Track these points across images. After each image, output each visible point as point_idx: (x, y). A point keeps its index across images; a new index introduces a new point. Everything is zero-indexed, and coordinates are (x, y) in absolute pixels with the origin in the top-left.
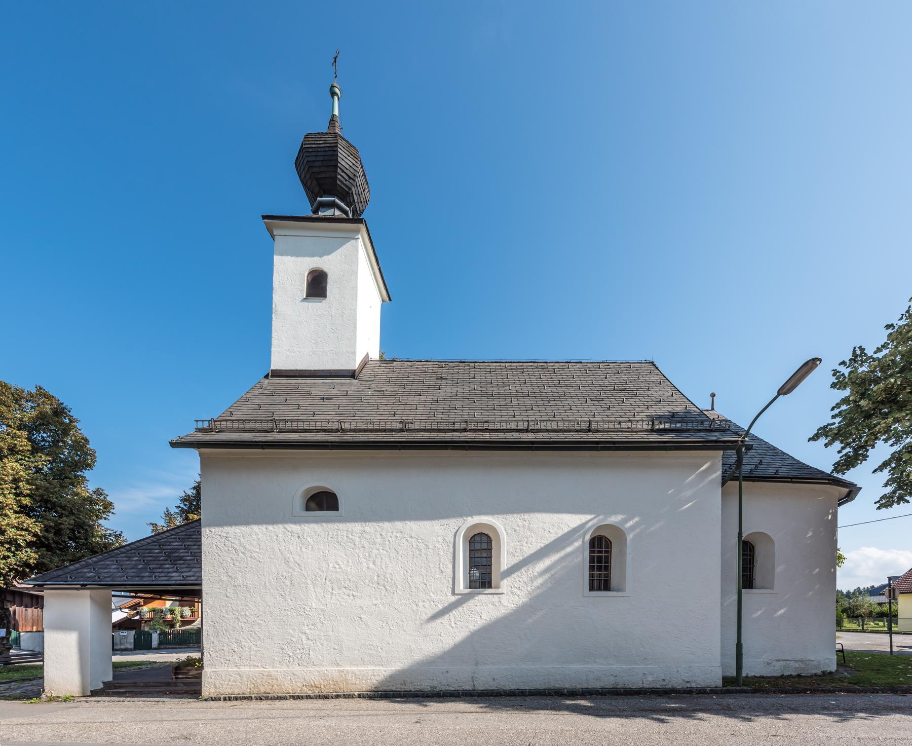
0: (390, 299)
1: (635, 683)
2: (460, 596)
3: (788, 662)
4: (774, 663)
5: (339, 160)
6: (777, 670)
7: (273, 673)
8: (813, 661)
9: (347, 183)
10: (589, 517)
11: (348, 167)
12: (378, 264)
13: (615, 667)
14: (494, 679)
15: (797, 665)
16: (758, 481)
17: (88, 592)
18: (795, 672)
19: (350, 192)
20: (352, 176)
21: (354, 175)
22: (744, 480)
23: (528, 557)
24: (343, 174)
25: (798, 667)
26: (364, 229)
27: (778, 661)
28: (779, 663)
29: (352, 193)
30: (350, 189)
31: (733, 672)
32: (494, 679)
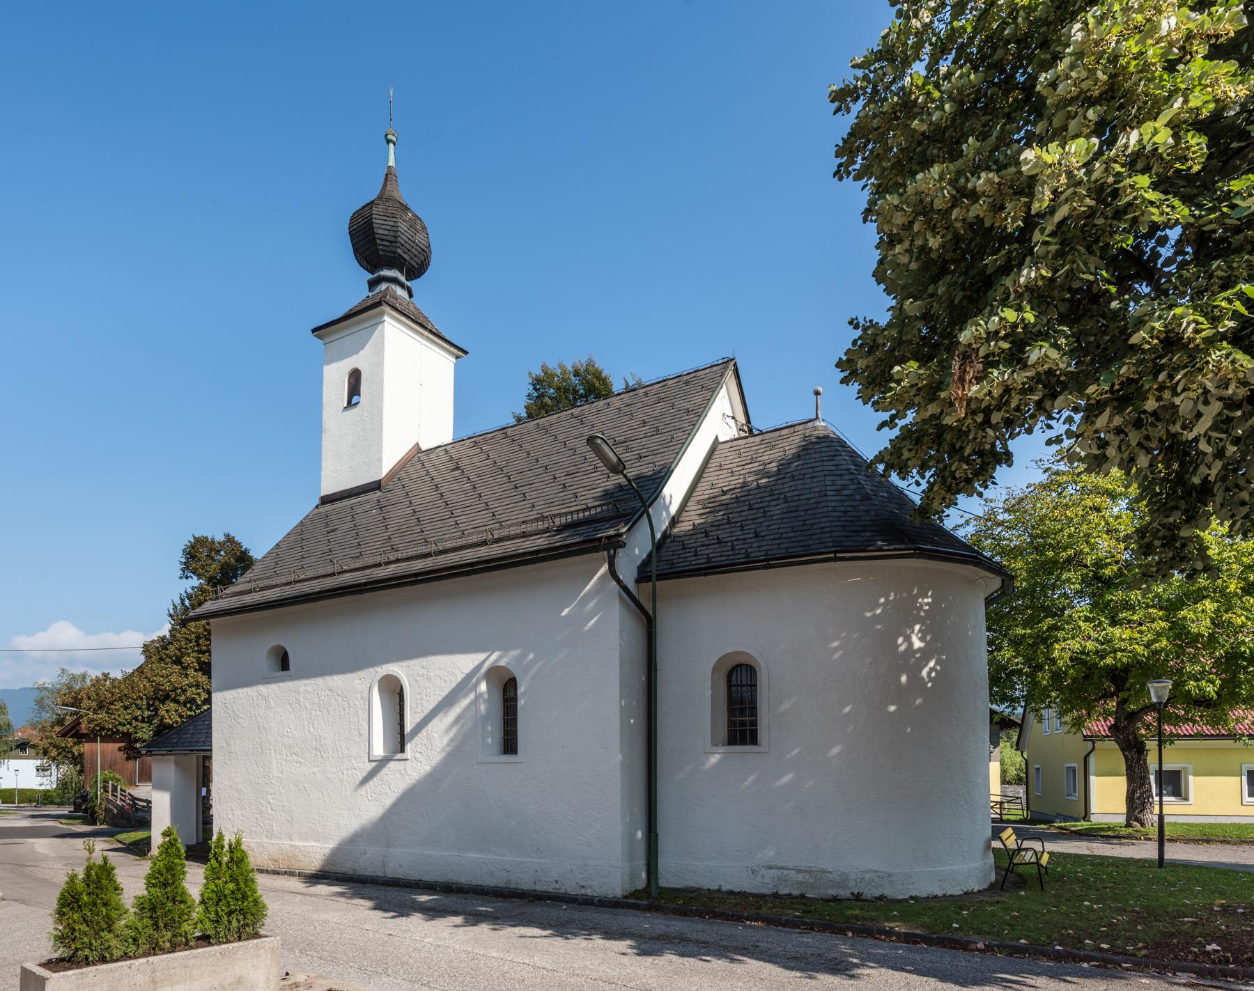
1: (526, 883)
2: (377, 763)
3: (785, 872)
4: (763, 871)
5: (376, 231)
7: (251, 844)
8: (830, 872)
9: (391, 249)
10: (481, 657)
11: (386, 233)
14: (400, 866)
15: (800, 877)
16: (690, 576)
17: (173, 758)
18: (796, 889)
20: (393, 239)
21: (395, 237)
22: (658, 580)
23: (429, 714)
25: (802, 882)
26: (387, 309)
27: (770, 868)
28: (770, 871)
29: (399, 255)
31: (641, 882)
32: (400, 866)
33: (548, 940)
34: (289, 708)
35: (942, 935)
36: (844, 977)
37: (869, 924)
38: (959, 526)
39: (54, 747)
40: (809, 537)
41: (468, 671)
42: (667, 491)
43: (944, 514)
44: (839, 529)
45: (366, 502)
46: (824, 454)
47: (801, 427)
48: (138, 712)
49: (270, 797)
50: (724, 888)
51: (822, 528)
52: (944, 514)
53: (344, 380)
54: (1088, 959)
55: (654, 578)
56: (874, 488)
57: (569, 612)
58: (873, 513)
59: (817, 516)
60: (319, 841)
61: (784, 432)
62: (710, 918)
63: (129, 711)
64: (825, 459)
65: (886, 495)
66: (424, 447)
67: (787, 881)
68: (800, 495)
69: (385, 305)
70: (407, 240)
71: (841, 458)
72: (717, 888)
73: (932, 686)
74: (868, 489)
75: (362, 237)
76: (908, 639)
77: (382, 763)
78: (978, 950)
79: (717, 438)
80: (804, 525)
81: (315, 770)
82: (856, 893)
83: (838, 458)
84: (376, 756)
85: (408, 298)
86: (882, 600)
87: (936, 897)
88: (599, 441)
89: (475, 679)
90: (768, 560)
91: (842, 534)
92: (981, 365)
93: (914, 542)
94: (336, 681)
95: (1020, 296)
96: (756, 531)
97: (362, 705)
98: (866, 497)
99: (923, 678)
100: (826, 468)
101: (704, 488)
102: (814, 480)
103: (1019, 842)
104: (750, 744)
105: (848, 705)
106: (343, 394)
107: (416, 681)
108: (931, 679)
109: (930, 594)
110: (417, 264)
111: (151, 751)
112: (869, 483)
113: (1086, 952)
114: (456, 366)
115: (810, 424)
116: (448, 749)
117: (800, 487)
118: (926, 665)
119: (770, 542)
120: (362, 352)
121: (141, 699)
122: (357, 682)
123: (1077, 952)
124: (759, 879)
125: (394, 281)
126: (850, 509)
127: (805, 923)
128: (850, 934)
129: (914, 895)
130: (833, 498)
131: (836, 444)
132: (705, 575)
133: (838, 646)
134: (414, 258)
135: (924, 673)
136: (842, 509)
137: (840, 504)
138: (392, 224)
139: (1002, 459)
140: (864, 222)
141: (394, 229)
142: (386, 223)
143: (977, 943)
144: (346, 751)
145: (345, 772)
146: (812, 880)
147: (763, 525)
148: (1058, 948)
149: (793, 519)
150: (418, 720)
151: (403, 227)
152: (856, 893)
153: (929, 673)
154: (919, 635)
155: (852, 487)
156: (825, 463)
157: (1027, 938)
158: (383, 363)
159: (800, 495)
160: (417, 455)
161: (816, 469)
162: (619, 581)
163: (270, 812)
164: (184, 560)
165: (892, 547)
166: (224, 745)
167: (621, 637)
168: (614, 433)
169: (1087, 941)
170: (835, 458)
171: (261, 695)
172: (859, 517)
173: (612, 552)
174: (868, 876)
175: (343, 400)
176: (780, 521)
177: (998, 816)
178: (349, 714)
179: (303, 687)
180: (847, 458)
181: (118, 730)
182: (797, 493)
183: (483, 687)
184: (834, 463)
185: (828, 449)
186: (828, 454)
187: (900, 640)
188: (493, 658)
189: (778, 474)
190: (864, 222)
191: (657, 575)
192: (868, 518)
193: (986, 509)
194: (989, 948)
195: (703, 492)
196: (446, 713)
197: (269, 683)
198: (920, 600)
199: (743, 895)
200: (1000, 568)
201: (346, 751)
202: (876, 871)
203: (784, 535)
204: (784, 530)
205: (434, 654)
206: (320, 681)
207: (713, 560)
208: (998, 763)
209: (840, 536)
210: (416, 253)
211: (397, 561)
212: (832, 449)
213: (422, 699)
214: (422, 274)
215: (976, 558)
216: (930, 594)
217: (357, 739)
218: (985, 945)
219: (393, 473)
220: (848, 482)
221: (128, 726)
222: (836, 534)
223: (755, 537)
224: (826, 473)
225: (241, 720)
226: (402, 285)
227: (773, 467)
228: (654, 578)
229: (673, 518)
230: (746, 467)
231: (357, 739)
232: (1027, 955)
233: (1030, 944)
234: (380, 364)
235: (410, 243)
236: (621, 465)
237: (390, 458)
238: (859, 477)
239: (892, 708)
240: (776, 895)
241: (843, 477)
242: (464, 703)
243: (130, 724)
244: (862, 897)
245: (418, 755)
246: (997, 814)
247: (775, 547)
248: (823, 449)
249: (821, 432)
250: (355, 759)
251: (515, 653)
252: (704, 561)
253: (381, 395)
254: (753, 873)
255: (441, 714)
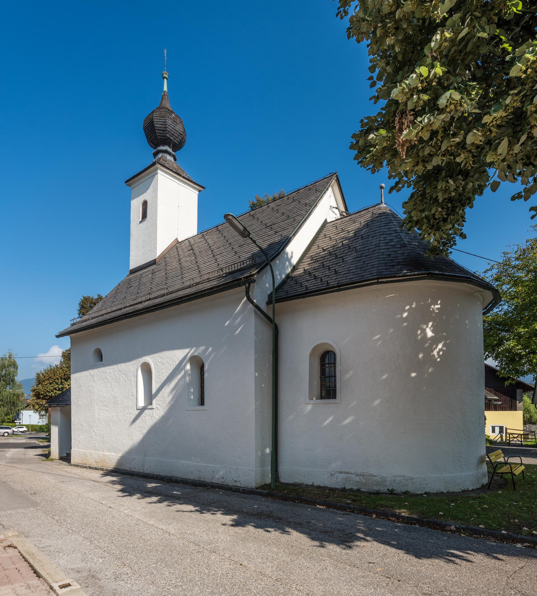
0: (204, 188)
1: (207, 477)
3: (349, 475)
5: (155, 125)
6: (339, 482)
8: (375, 476)
10: (187, 351)
11: (161, 126)
12: (181, 175)
13: (199, 464)
15: (358, 479)
17: (59, 408)
19: (167, 138)
20: (164, 129)
21: (165, 128)
22: (276, 303)
24: (160, 132)
26: (158, 166)
27: (341, 473)
28: (341, 474)
30: (166, 136)
33: (194, 515)
34: (103, 381)
35: (430, 520)
36: (344, 547)
37: (387, 510)
38: (488, 270)
39: (37, 404)
40: (364, 271)
41: (180, 359)
42: (289, 249)
43: (449, 252)
44: (383, 265)
45: (148, 271)
46: (382, 223)
47: (372, 209)
48: (57, 386)
49: (95, 429)
50: (315, 484)
51: (373, 265)
52: (449, 252)
53: (139, 208)
54: (522, 541)
55: (274, 301)
56: (410, 240)
57: (229, 323)
58: (406, 254)
59: (372, 259)
60: (115, 452)
61: (362, 213)
62: (298, 502)
63: (52, 385)
64: (382, 225)
65: (417, 244)
66: (180, 240)
67: (351, 481)
68: (364, 247)
69: (158, 164)
70: (172, 129)
71: (393, 224)
72: (311, 484)
73: (440, 360)
74: (406, 240)
75: (149, 130)
76: (424, 331)
77: (143, 409)
78: (451, 531)
79: (326, 220)
80: (363, 264)
81: (113, 414)
82: (390, 489)
83: (391, 224)
84: (140, 407)
85: (173, 161)
86: (408, 307)
87: (442, 493)
88: (230, 217)
89: (184, 363)
90: (339, 286)
91: (384, 267)
92: (412, 117)
93: (427, 269)
94: (122, 366)
95: (434, 59)
96: (335, 271)
97: (133, 379)
98: (404, 246)
99: (434, 355)
100: (382, 230)
101: (314, 249)
102: (374, 238)
103: (506, 458)
104: (333, 399)
105: (386, 373)
106: (139, 215)
107: (157, 366)
108: (439, 356)
109: (439, 302)
110: (178, 142)
111: (50, 405)
112: (407, 238)
113: (522, 536)
114: (199, 195)
115: (377, 207)
116: (172, 403)
117: (365, 243)
118: (436, 348)
119: (342, 276)
120: (148, 191)
121: (58, 379)
122: (131, 366)
123: (516, 535)
124: (334, 479)
125: (166, 152)
126: (392, 253)
127: (350, 508)
128: (374, 516)
129: (427, 491)
130: (383, 247)
131: (390, 216)
132: (304, 297)
133: (379, 338)
134: (176, 139)
135: (435, 353)
136: (388, 253)
137: (387, 250)
138: (163, 121)
139: (465, 203)
140: (349, 38)
141: (165, 123)
142: (161, 120)
143: (451, 526)
144: (126, 404)
145: (126, 415)
146: (364, 481)
147: (341, 266)
148: (503, 532)
149: (358, 262)
150: (158, 387)
151: (169, 122)
152: (390, 489)
153: (438, 353)
154: (432, 328)
155: (396, 240)
156: (382, 228)
157: (485, 524)
158: (157, 196)
159: (364, 247)
160: (177, 244)
161: (376, 232)
162: (252, 302)
163: (95, 437)
164: (79, 309)
165: (413, 273)
166: (76, 401)
167: (255, 334)
168: (268, 221)
169: (525, 528)
170: (389, 224)
171: (91, 375)
172: (397, 257)
173: (247, 285)
174: (398, 479)
175: (139, 218)
176: (351, 263)
177: (520, 443)
178: (128, 384)
179: (108, 370)
180: (396, 224)
181: (47, 395)
182: (363, 246)
183: (188, 367)
184: (388, 227)
185: (385, 220)
186: (384, 222)
187: (419, 332)
188: (192, 351)
189: (355, 237)
190: (349, 38)
191: (276, 300)
192: (403, 257)
193: (504, 258)
194: (458, 530)
195: (314, 251)
196: (170, 382)
197: (94, 368)
198: (432, 307)
199: (324, 488)
200: (487, 285)
201: (126, 404)
202: (403, 476)
203: (351, 271)
204: (351, 268)
205: (165, 350)
206: (115, 367)
207: (309, 288)
208: (522, 412)
209: (383, 269)
210: (177, 136)
211: (150, 299)
212: (387, 219)
213: (160, 375)
214: (182, 147)
215: (470, 278)
216: (439, 302)
217: (132, 398)
218: (456, 527)
219: (163, 256)
220: (394, 238)
221: (52, 393)
222: (380, 268)
223: (335, 273)
224: (382, 233)
225: (83, 388)
226: (170, 154)
227: (351, 234)
228: (274, 301)
229: (294, 267)
230: (338, 235)
231: (132, 398)
232: (482, 536)
233: (486, 529)
234: (156, 196)
235: (174, 130)
236: (247, 232)
237: (161, 249)
238: (401, 234)
239: (413, 375)
240: (344, 490)
241: (391, 235)
242: (179, 376)
243: (52, 391)
244: (394, 492)
245: (158, 406)
246: (519, 441)
247: (344, 278)
248: (382, 220)
249: (382, 210)
250: (131, 408)
251: (202, 348)
252: (304, 289)
253: (156, 213)
254: (331, 476)
255: (168, 383)
